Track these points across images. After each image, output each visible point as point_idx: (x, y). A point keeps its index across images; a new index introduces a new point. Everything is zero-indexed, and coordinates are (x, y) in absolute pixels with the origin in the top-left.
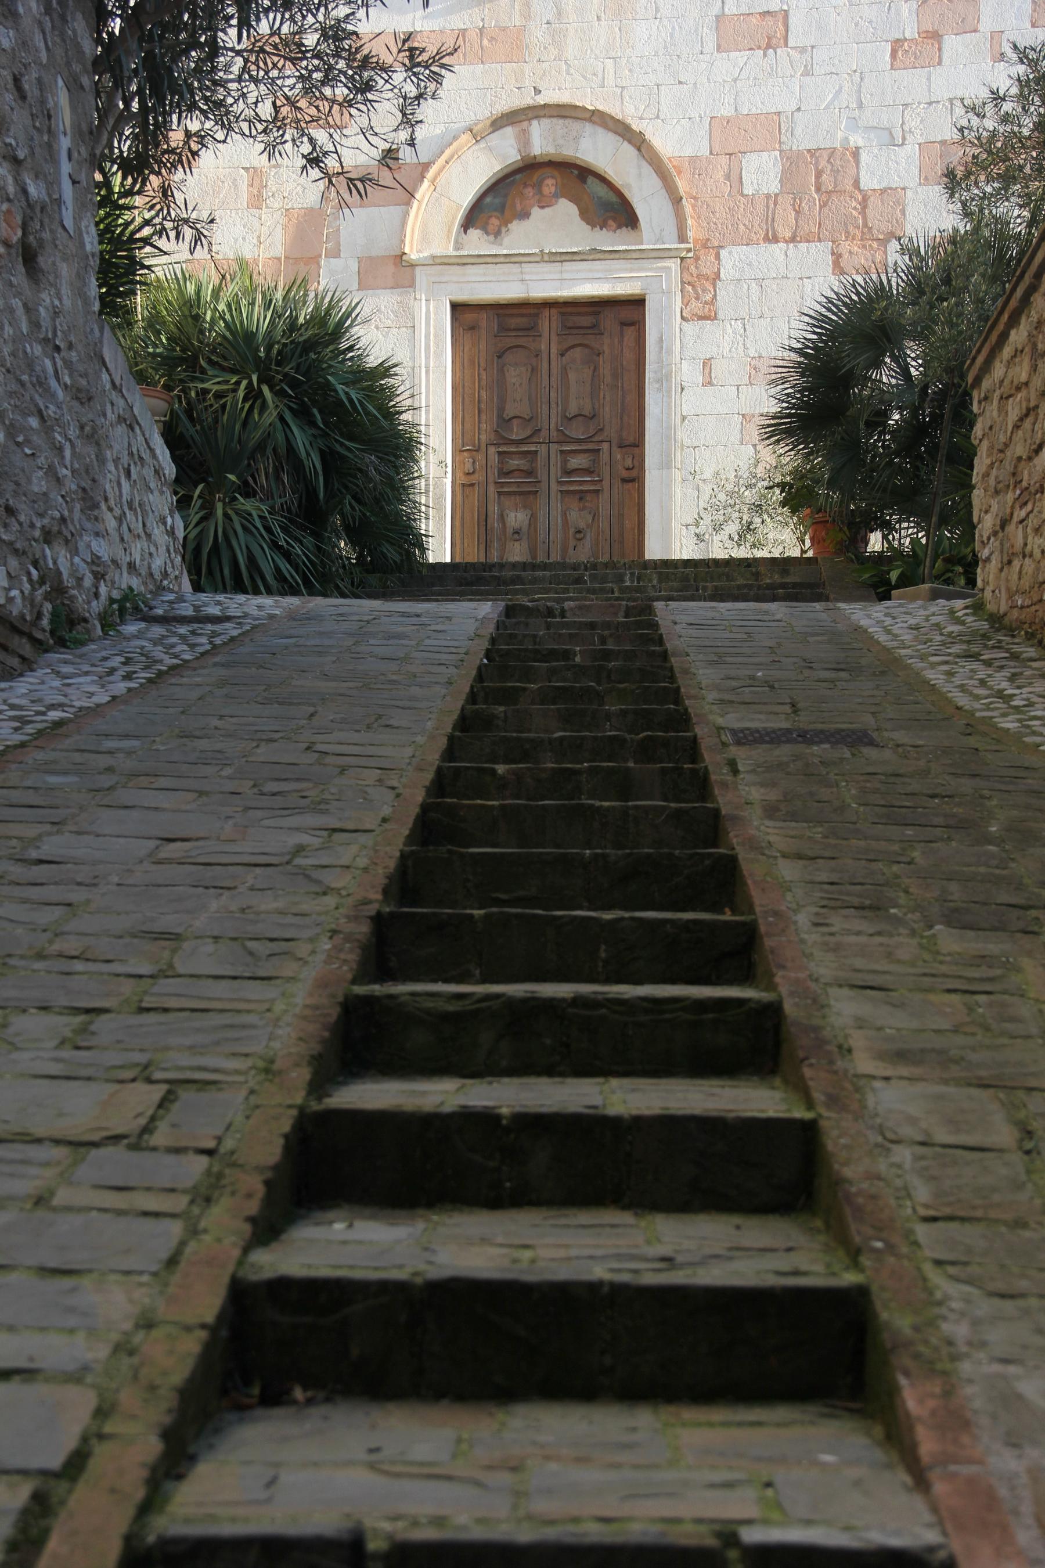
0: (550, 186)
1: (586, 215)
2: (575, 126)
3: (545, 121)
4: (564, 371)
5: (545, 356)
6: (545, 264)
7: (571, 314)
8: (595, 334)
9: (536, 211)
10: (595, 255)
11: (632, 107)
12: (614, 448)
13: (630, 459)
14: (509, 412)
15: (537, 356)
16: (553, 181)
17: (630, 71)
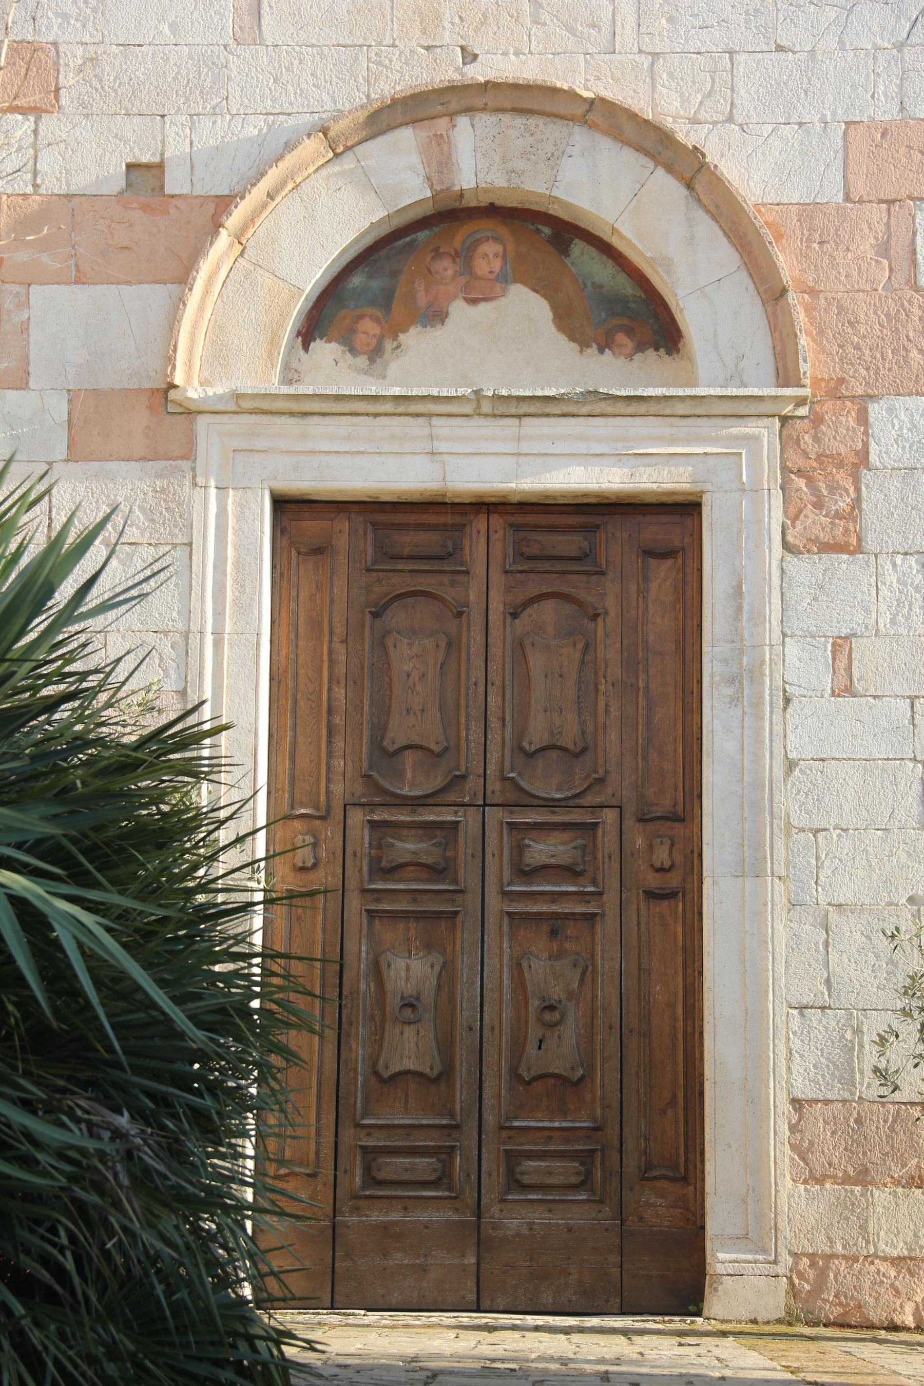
0: (490, 256)
1: (564, 320)
2: (551, 131)
3: (485, 120)
4: (520, 646)
5: (476, 616)
6: (482, 421)
7: (535, 528)
8: (587, 573)
9: (459, 309)
10: (595, 404)
11: (675, 96)
12: (629, 822)
13: (666, 848)
14: (399, 733)
15: (460, 614)
16: (499, 248)
17: (671, 20)
